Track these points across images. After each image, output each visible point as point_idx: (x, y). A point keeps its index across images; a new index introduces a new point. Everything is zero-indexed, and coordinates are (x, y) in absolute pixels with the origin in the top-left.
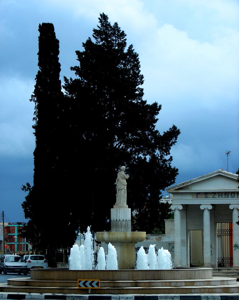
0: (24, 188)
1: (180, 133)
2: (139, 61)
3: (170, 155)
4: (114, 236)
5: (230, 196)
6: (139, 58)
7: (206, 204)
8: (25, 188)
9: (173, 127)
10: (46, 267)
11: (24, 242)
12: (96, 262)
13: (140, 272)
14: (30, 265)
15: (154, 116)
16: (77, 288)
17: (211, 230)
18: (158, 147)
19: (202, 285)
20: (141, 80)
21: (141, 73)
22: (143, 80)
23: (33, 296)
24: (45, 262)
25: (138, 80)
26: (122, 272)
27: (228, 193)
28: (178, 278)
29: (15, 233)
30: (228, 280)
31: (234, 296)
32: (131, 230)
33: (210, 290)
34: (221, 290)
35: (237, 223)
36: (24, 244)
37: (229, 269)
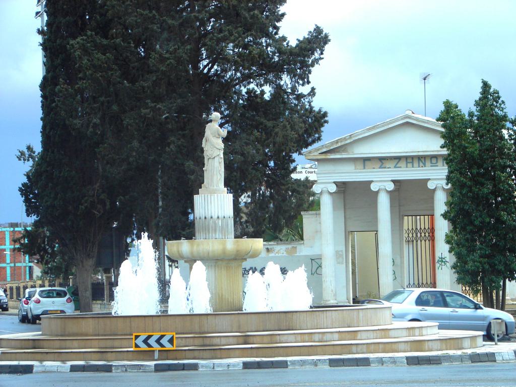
0: (21, 156)
3: (310, 86)
5: (428, 163)
8: (24, 155)
9: (315, 30)
10: (70, 311)
11: (25, 261)
12: (165, 299)
13: (253, 315)
14: (38, 309)
15: (277, 8)
17: (392, 230)
18: (287, 69)
19: (372, 337)
23: (47, 366)
24: (69, 301)
26: (217, 317)
27: (425, 157)
28: (325, 325)
29: (5, 245)
30: (422, 327)
31: (431, 356)
32: (233, 237)
33: (388, 347)
34: (408, 347)
35: (442, 215)
36: (25, 267)
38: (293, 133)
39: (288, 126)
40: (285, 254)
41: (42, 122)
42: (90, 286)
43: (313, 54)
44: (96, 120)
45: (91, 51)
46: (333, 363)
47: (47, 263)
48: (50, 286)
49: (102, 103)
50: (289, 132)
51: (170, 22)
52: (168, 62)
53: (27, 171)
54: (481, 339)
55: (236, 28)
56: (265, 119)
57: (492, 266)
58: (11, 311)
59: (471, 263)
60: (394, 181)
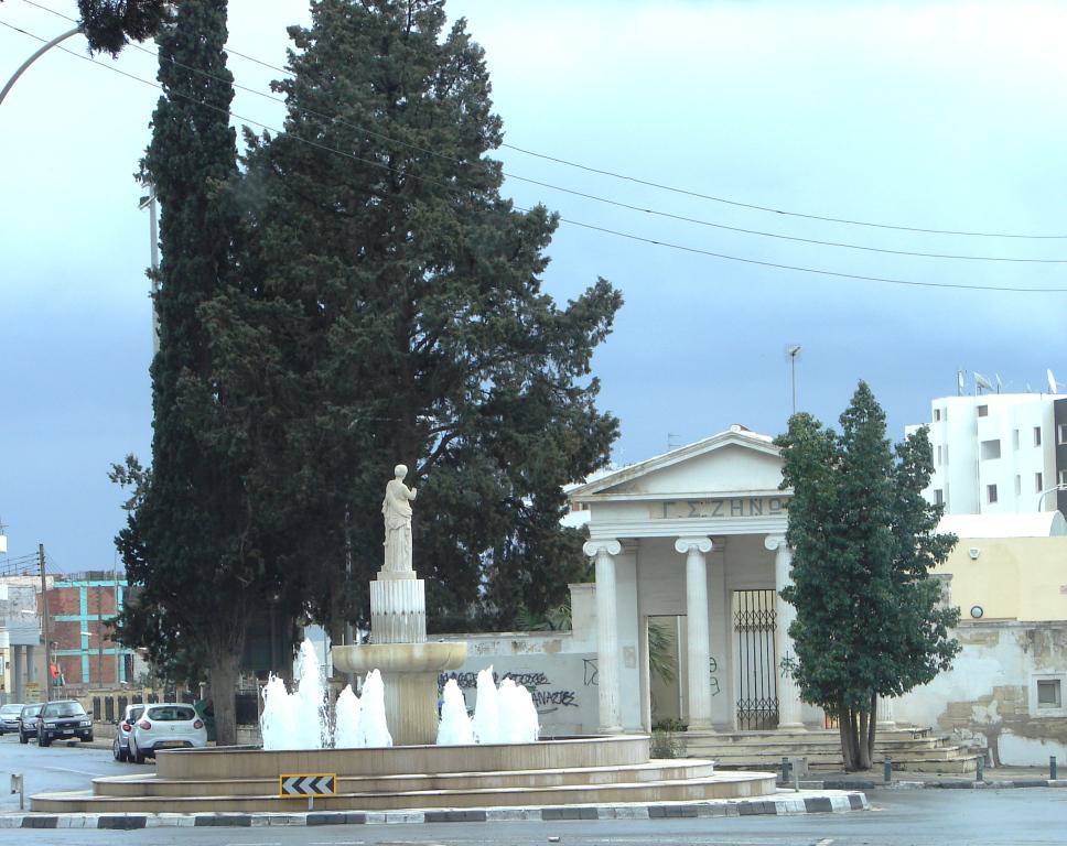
0: (118, 475)
1: (622, 303)
2: (487, 71)
4: (378, 657)
6: (485, 63)
7: (693, 536)
9: (598, 285)
14: (149, 738)
15: (537, 249)
16: (278, 797)
20: (495, 133)
21: (493, 111)
22: (501, 131)
24: (197, 725)
25: (483, 133)
29: (79, 614)
37: (768, 736)
38: (562, 453)
39: (554, 444)
40: (543, 652)
41: (153, 429)
42: (232, 702)
43: (595, 323)
44: (242, 434)
45: (232, 321)
46: (547, 814)
47: (161, 661)
48: (167, 699)
49: (252, 407)
50: (555, 451)
51: (363, 274)
52: (360, 339)
53: (127, 500)
54: (774, 782)
55: (470, 283)
56: (517, 431)
57: (854, 673)
58: (97, 741)
59: (820, 670)
60: (711, 537)
